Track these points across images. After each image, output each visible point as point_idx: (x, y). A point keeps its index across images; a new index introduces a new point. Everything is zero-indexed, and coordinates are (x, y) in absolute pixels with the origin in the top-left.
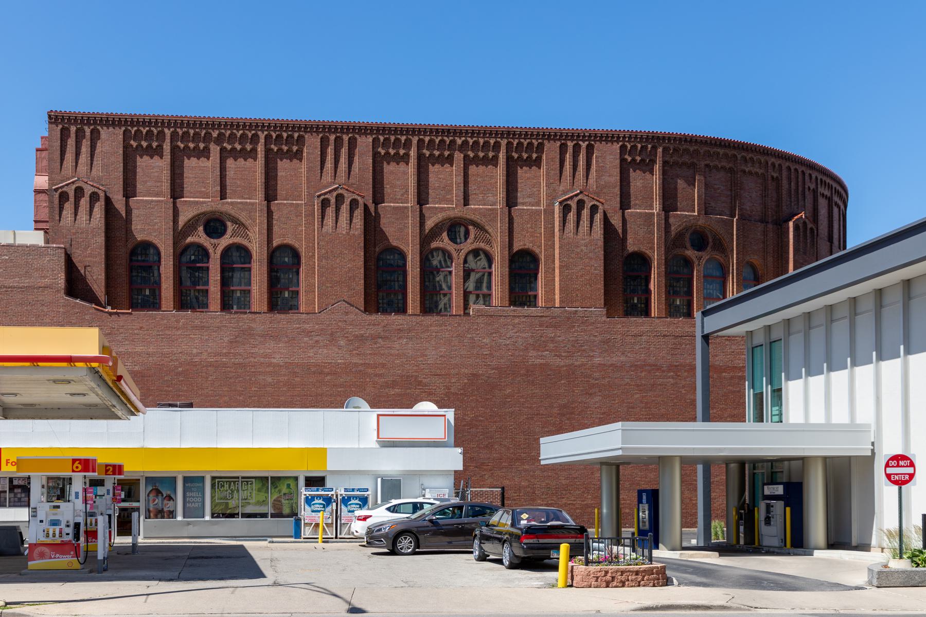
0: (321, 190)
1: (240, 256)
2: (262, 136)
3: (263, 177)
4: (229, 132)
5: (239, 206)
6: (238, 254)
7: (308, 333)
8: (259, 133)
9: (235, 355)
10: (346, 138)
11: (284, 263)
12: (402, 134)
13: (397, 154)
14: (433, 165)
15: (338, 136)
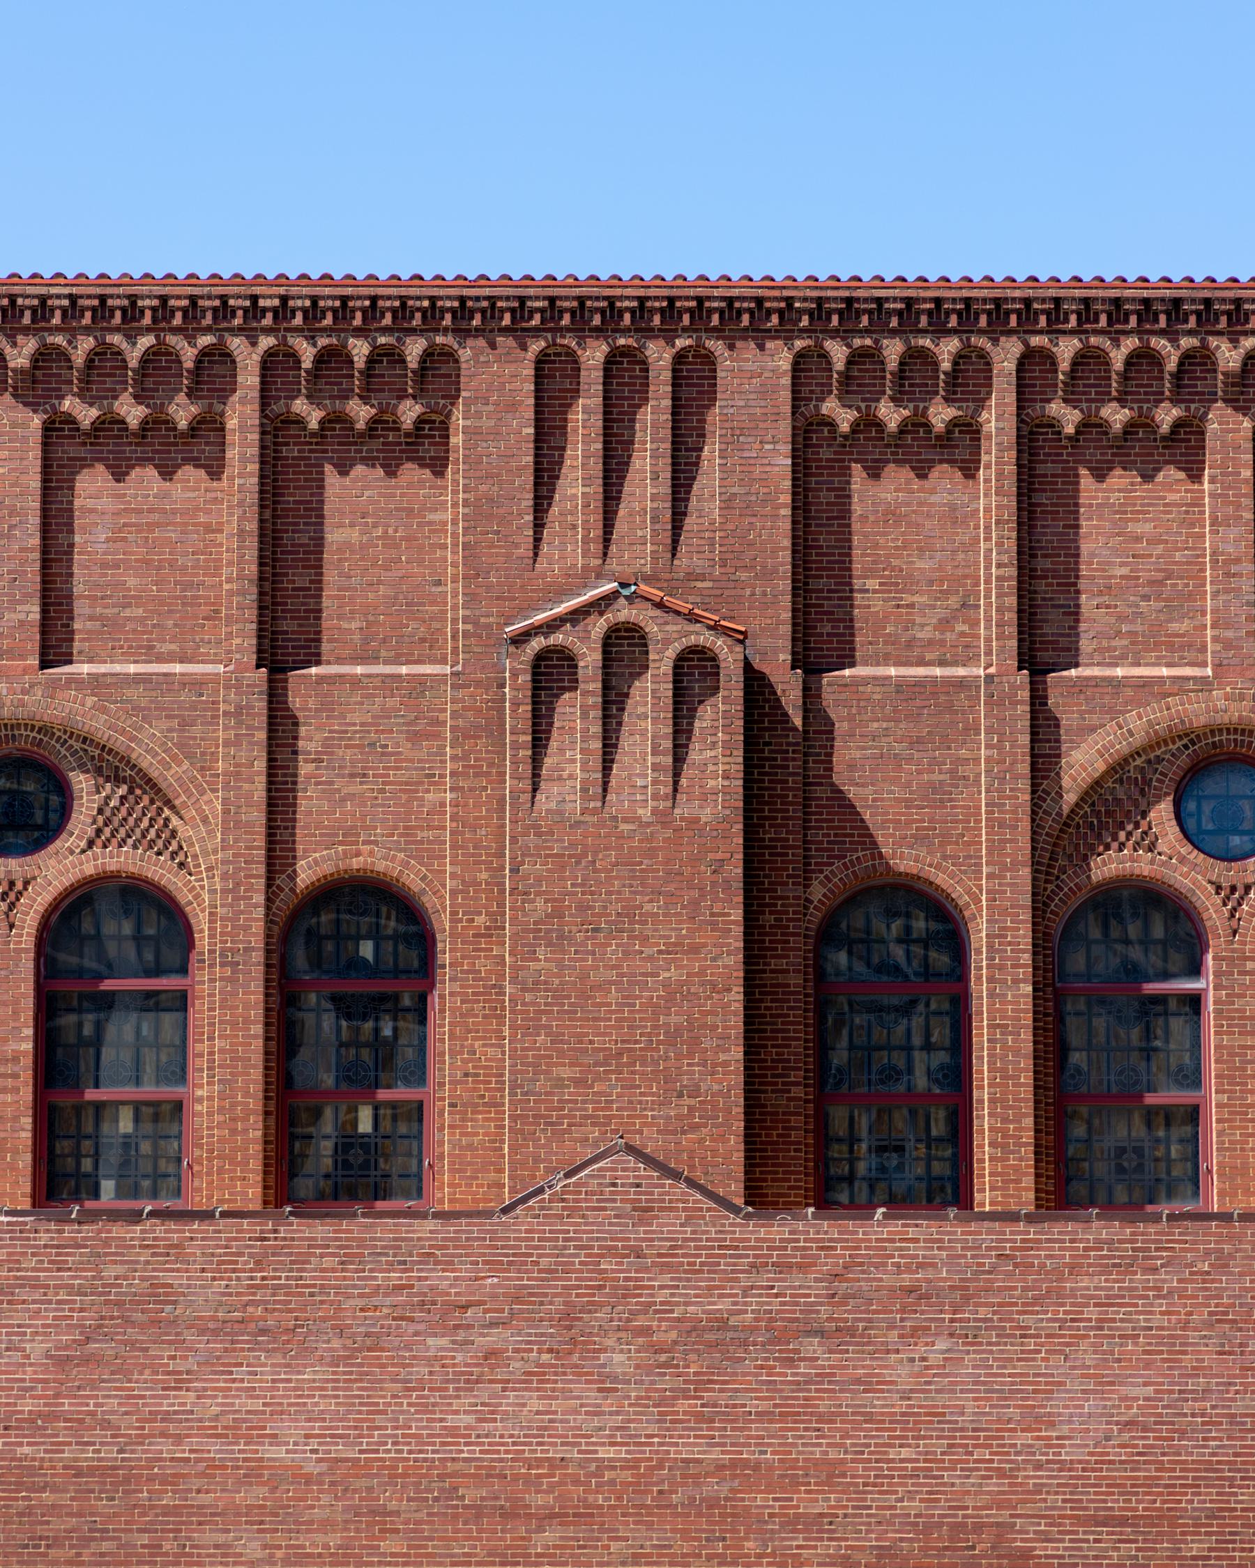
0: (524, 612)
1: (138, 938)
2: (248, 358)
3: (252, 554)
4: (86, 344)
5: (134, 694)
6: (127, 928)
7: (450, 1314)
8: (236, 344)
9: (78, 1423)
10: (659, 355)
11: (353, 963)
12: (940, 331)
13: (916, 425)
14: (1100, 476)
15: (623, 351)
